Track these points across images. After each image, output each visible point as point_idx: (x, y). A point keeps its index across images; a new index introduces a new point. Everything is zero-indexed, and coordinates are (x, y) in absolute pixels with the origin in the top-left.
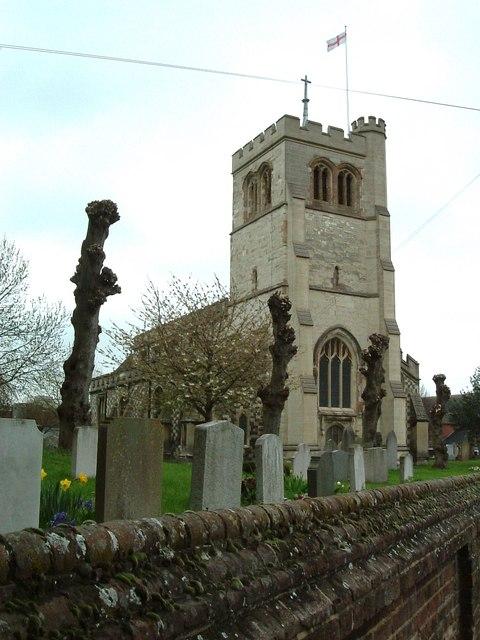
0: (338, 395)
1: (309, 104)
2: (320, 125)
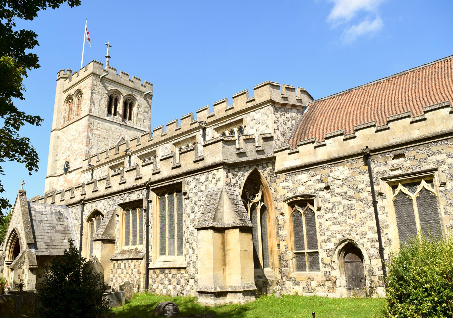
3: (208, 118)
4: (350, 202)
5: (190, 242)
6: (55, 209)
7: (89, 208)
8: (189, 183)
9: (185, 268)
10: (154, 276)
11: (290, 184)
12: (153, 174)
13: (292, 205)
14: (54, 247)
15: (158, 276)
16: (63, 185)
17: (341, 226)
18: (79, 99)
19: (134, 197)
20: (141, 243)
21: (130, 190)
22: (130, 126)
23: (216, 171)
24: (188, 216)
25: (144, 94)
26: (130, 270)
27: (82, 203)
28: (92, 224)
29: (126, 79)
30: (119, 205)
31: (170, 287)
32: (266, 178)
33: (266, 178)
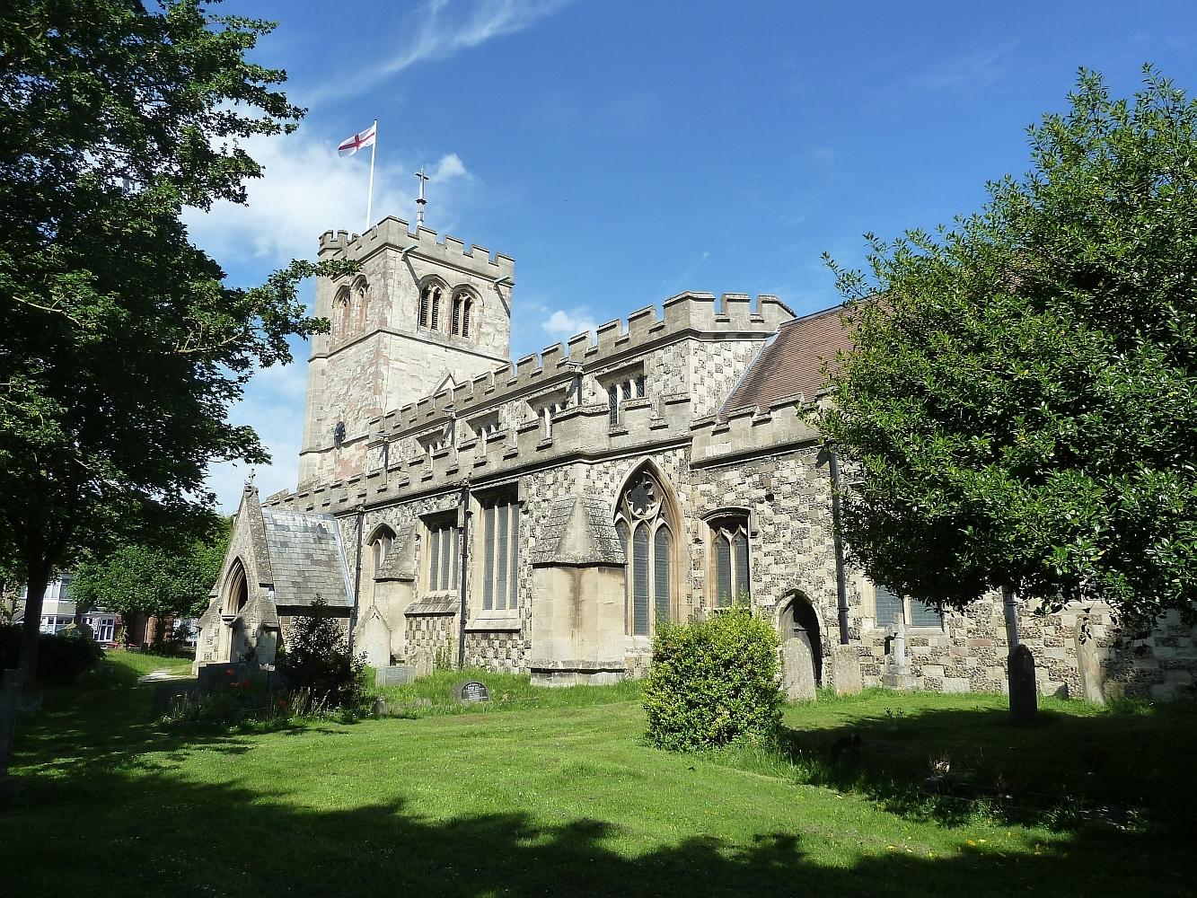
3: (587, 355)
4: (802, 526)
5: (528, 586)
6: (312, 520)
7: (370, 523)
8: (528, 486)
10: (473, 644)
11: (712, 488)
12: (476, 466)
13: (714, 525)
14: (308, 590)
18: (362, 296)
19: (446, 503)
21: (439, 492)
22: (466, 349)
23: (570, 466)
24: (527, 541)
25: (495, 281)
26: (435, 634)
27: (358, 513)
28: (377, 551)
29: (458, 252)
30: (422, 518)
31: (496, 663)
32: (670, 476)
33: (670, 476)
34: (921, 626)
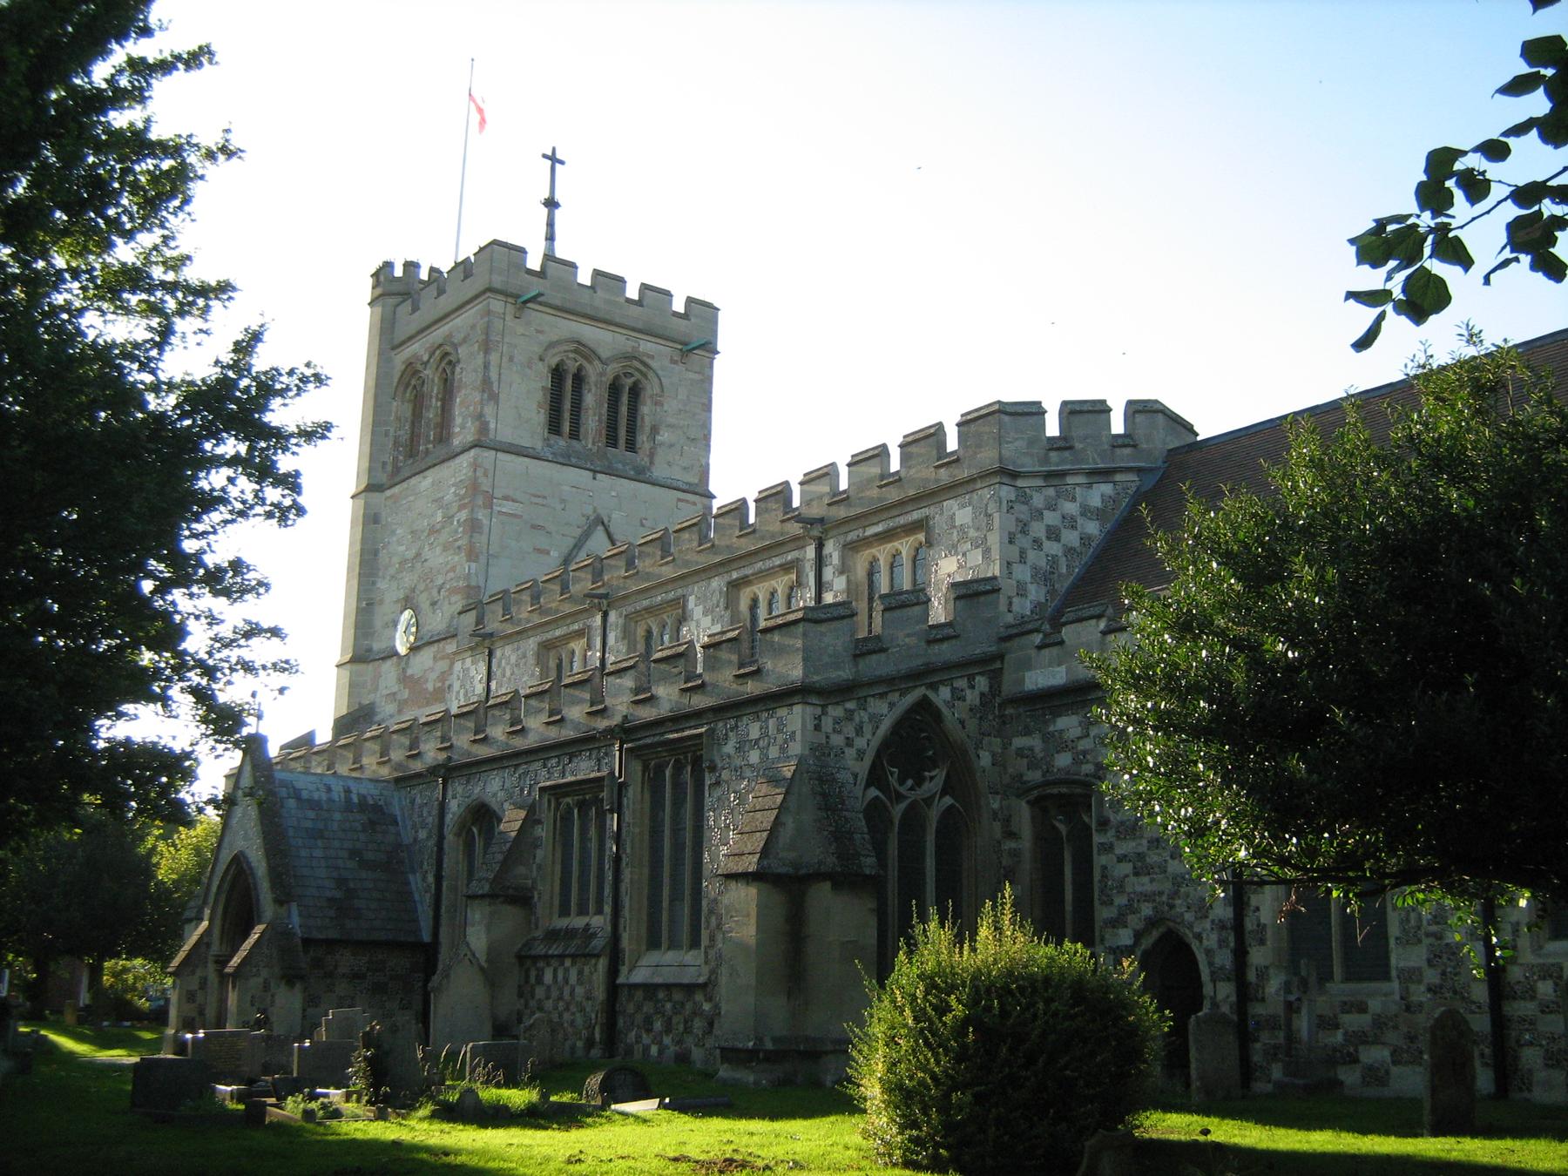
0: (1076, 899)
1: (558, 212)
2: (621, 281)
9: (704, 986)
11: (1035, 742)
15: (639, 1008)
16: (394, 694)
17: (1152, 881)
20: (600, 911)
21: (569, 749)
32: (962, 722)
34: (1360, 979)
